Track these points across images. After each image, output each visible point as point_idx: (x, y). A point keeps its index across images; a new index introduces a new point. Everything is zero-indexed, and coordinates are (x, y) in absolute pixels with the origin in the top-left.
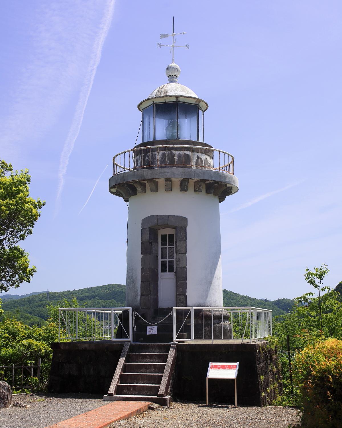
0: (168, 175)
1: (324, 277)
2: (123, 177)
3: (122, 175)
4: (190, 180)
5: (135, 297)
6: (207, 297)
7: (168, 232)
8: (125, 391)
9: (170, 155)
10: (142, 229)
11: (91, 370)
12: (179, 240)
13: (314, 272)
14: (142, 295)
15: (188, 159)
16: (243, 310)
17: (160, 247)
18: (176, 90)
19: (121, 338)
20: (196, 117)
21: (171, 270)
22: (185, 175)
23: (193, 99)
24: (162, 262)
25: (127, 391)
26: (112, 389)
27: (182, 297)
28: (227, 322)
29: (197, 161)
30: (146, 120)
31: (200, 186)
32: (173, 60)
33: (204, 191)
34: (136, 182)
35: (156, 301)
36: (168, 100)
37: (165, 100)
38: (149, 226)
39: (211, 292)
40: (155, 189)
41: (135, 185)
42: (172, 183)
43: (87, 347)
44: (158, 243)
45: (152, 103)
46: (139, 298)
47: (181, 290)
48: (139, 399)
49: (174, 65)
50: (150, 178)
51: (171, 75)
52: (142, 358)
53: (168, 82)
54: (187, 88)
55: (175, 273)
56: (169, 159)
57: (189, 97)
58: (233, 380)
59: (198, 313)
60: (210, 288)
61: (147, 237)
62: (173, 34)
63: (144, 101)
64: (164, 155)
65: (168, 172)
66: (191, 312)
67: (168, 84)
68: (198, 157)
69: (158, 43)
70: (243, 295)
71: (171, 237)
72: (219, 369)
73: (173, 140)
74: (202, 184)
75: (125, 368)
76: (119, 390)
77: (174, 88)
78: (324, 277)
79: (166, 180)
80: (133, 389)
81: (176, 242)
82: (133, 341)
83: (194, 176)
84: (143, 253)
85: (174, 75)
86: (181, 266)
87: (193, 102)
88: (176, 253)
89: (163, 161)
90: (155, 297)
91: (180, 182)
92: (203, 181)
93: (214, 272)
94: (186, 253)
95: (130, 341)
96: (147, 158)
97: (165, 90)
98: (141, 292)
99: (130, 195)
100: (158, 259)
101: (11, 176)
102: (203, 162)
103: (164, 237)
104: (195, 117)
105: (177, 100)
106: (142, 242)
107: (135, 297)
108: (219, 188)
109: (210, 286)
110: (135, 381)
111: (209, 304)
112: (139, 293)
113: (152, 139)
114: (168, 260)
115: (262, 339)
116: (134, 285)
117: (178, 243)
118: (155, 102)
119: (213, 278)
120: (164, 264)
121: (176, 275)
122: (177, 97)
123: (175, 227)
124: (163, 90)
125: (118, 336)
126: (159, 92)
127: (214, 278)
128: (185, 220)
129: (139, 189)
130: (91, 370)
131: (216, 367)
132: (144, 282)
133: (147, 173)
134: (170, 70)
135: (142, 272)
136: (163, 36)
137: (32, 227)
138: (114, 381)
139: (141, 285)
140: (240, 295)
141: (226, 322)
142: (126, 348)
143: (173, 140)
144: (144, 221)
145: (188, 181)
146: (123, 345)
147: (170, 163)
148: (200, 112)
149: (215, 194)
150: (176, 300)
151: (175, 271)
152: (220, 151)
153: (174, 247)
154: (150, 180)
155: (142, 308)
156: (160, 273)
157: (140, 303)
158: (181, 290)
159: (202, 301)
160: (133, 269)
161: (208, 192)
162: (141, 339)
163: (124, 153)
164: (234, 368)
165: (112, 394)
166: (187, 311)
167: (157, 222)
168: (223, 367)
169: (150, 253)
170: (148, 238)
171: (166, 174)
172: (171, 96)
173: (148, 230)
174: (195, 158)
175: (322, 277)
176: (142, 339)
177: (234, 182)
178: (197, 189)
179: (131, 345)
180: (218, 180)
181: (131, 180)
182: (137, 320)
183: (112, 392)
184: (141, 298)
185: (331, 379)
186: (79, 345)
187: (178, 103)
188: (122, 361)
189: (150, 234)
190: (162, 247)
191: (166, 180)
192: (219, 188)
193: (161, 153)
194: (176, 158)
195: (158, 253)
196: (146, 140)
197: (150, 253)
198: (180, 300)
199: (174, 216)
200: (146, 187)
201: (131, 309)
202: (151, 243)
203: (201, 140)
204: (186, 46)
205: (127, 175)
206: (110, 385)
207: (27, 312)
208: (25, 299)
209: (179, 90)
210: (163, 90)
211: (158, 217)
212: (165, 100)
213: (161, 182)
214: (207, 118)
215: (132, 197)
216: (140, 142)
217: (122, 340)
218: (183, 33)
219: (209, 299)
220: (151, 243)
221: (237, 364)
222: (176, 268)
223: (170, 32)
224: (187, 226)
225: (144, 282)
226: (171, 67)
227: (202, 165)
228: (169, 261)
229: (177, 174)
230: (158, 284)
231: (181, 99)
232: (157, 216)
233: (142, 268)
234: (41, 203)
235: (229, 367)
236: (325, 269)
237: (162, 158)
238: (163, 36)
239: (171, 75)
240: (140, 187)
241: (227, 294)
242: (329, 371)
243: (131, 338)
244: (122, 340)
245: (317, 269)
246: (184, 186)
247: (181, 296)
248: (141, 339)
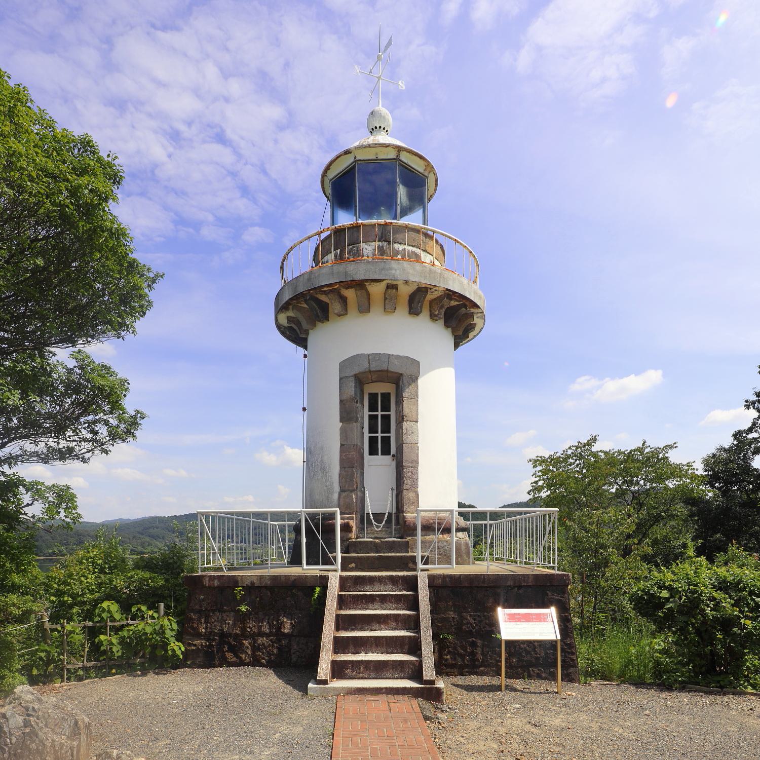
5: (329, 494)
10: (341, 379)
19: (390, 415)
21: (386, 451)
23: (421, 162)
25: (353, 671)
26: (324, 669)
38: (353, 373)
40: (365, 308)
43: (255, 581)
46: (336, 496)
48: (384, 690)
52: (366, 602)
55: (393, 456)
72: (519, 621)
80: (365, 667)
84: (342, 420)
94: (417, 422)
98: (340, 485)
103: (373, 397)
105: (397, 156)
106: (341, 401)
107: (329, 494)
112: (337, 488)
114: (379, 435)
115: (493, 555)
116: (326, 475)
118: (358, 158)
120: (373, 441)
129: (335, 307)
132: (345, 468)
135: (341, 452)
139: (340, 475)
144: (343, 365)
145: (427, 292)
160: (322, 448)
165: (325, 682)
167: (370, 366)
168: (527, 618)
170: (353, 393)
173: (352, 379)
176: (353, 565)
183: (326, 677)
186: (239, 578)
199: (398, 357)
205: (317, 275)
207: (139, 533)
208: (136, 522)
211: (370, 357)
215: (319, 325)
225: (345, 468)
228: (382, 437)
232: (369, 355)
233: (342, 445)
235: (539, 618)
240: (339, 302)
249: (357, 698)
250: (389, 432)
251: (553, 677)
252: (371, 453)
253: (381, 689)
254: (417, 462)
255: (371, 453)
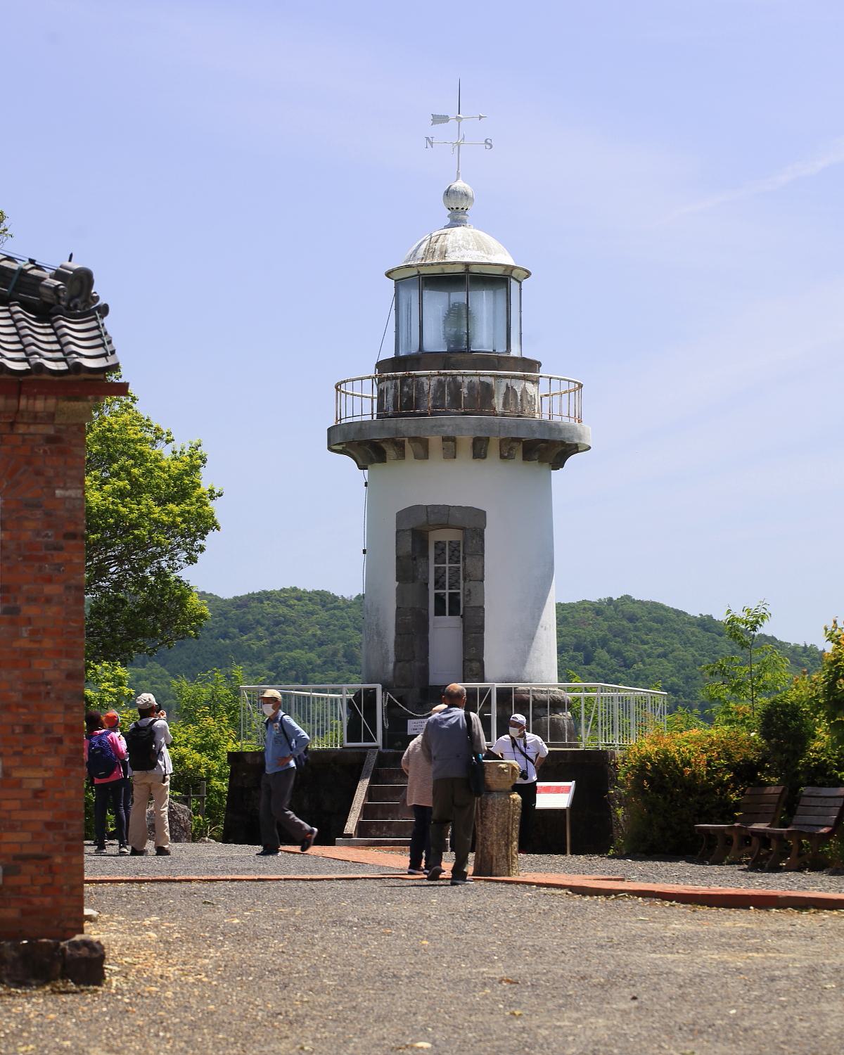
0: (449, 432)
1: (761, 625)
2: (360, 430)
3: (358, 426)
4: (491, 438)
6: (524, 664)
7: (446, 536)
8: (373, 831)
9: (452, 385)
10: (397, 532)
11: (305, 801)
12: (471, 555)
13: (743, 616)
14: (398, 661)
15: (487, 392)
16: (586, 690)
17: (432, 566)
18: (469, 246)
20: (505, 289)
22: (481, 430)
24: (436, 595)
26: (351, 826)
27: (475, 665)
28: (565, 714)
29: (506, 395)
30: (403, 293)
31: (511, 449)
32: (458, 173)
33: (519, 456)
34: (385, 440)
35: (425, 671)
36: (449, 270)
37: (443, 269)
38: (411, 526)
39: (534, 655)
41: (383, 445)
42: (455, 446)
44: (428, 557)
45: (416, 273)
46: (391, 666)
47: (473, 651)
49: (460, 185)
50: (413, 435)
51: (455, 208)
53: (448, 221)
54: (482, 234)
55: (462, 616)
56: (450, 394)
57: (490, 264)
58: (562, 811)
59: (504, 695)
60: (530, 647)
61: (408, 547)
62: (458, 118)
63: (399, 268)
64: (440, 384)
65: (450, 423)
66: (490, 694)
67: (445, 231)
68: (507, 387)
69: (427, 138)
70: (797, 646)
71: (455, 547)
73: (460, 353)
74: (515, 444)
75: (370, 794)
76: (362, 829)
77: (461, 242)
78: (761, 625)
79: (445, 439)
81: (464, 559)
82: (384, 748)
83: (499, 432)
85: (460, 208)
86: (472, 604)
87: (499, 271)
88: (465, 579)
89: (439, 396)
90: (424, 664)
91: (472, 441)
92: (518, 440)
93: (540, 616)
94: (482, 580)
95: (377, 747)
96: (406, 389)
97: (442, 246)
99: (372, 461)
100: (428, 590)
101: (173, 452)
102: (519, 394)
104: (501, 294)
106: (397, 558)
108: (552, 449)
109: (531, 643)
110: (390, 814)
111: (527, 678)
112: (392, 658)
113: (414, 349)
117: (467, 561)
118: (422, 273)
119: (537, 627)
120: (439, 599)
121: (464, 622)
122: (467, 265)
123: (463, 529)
124: (437, 246)
125: (353, 734)
126: (430, 251)
127: (539, 627)
128: (482, 514)
129: (391, 452)
130: (305, 801)
131: (547, 790)
133: (407, 426)
134: (453, 197)
136: (439, 119)
137: (203, 538)
138: (352, 815)
139: (396, 642)
140: (781, 643)
141: (561, 714)
142: (372, 759)
143: (460, 353)
144: (402, 516)
146: (365, 755)
147: (451, 406)
148: (514, 285)
149: (542, 460)
150: (464, 671)
151: (461, 613)
152: (551, 378)
153: (461, 565)
154: (414, 439)
155: (398, 687)
156: (433, 618)
157: (394, 676)
158: (473, 651)
159: (513, 673)
160: (378, 610)
161: (527, 457)
162: (397, 744)
163: (362, 379)
164: (567, 790)
165: (350, 836)
166: (484, 691)
167: (427, 519)
169: (414, 579)
170: (410, 549)
171: (445, 428)
172: (454, 263)
173: (409, 533)
174: (503, 390)
175: (758, 626)
176: (400, 743)
177: (580, 437)
178: (506, 454)
179: (379, 752)
180: (546, 438)
181: (375, 436)
182: (390, 706)
184: (395, 665)
185: (649, 767)
187: (468, 276)
188: (363, 786)
189: (413, 542)
190: (436, 563)
191: (445, 439)
192: (552, 449)
193: (434, 381)
194: (465, 391)
195: (427, 578)
196: (402, 353)
197: (414, 579)
198: (471, 670)
200: (404, 448)
201: (379, 687)
202: (415, 559)
203: (515, 352)
204: (486, 141)
206: (346, 821)
209: (471, 247)
210: (437, 246)
211: (429, 510)
212: (443, 269)
213: (435, 442)
214: (529, 295)
216: (389, 353)
217: (362, 744)
218: (481, 117)
219: (528, 668)
220: (415, 559)
221: (572, 784)
222: (464, 608)
223: (452, 113)
224: (485, 527)
225: (400, 634)
226: (455, 192)
227: (516, 403)
229: (466, 426)
230: (428, 638)
231: (474, 269)
232: (427, 506)
233: (398, 608)
234: (165, 457)
235: (558, 790)
236: (764, 611)
237: (436, 391)
238: (439, 119)
239: (455, 208)
241: (714, 640)
242: (649, 758)
243: (379, 742)
244: (362, 744)
245: (749, 611)
246: (479, 449)
247: (473, 665)
248: (397, 744)
249: (680, 908)
250: (436, 594)
251: (564, 853)
252: (436, 614)
253: (599, 890)
254: (482, 627)
255: (436, 614)
